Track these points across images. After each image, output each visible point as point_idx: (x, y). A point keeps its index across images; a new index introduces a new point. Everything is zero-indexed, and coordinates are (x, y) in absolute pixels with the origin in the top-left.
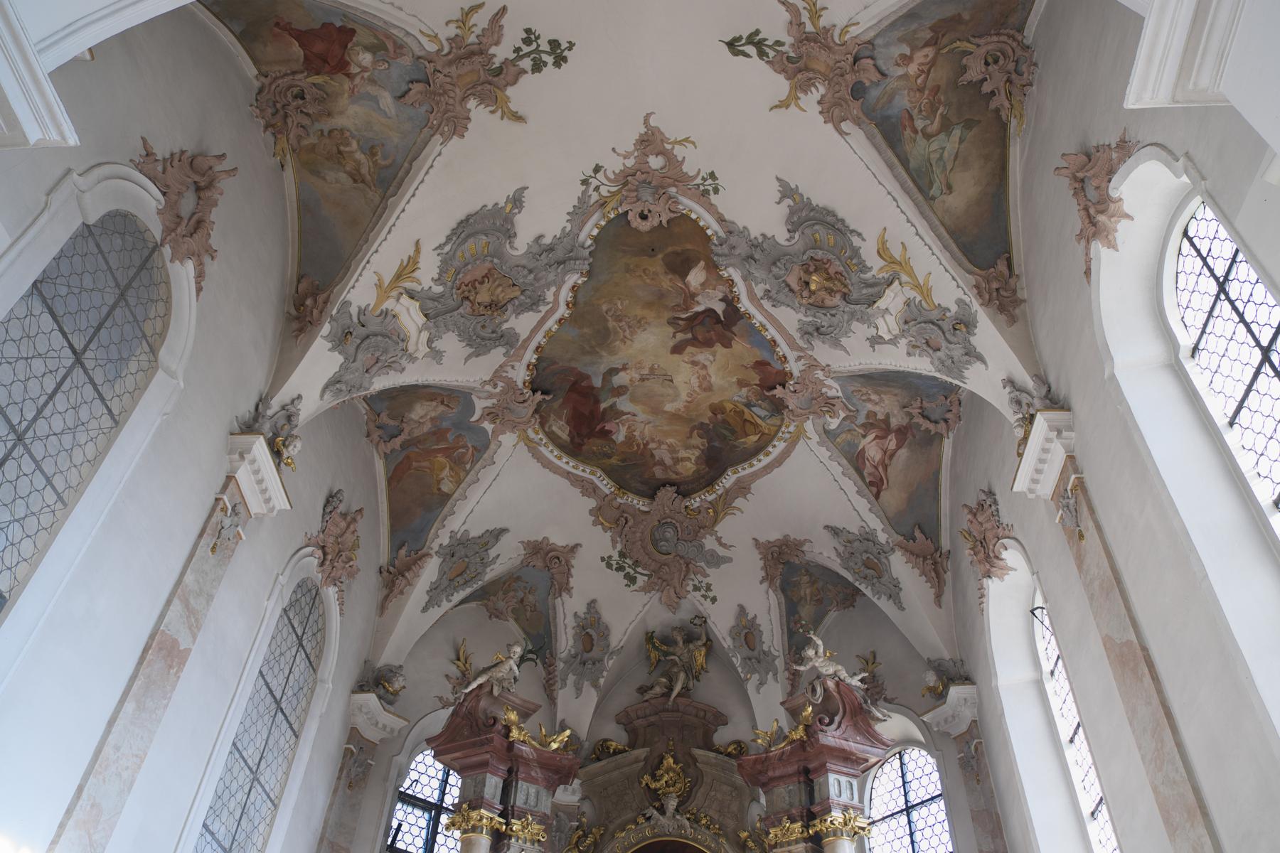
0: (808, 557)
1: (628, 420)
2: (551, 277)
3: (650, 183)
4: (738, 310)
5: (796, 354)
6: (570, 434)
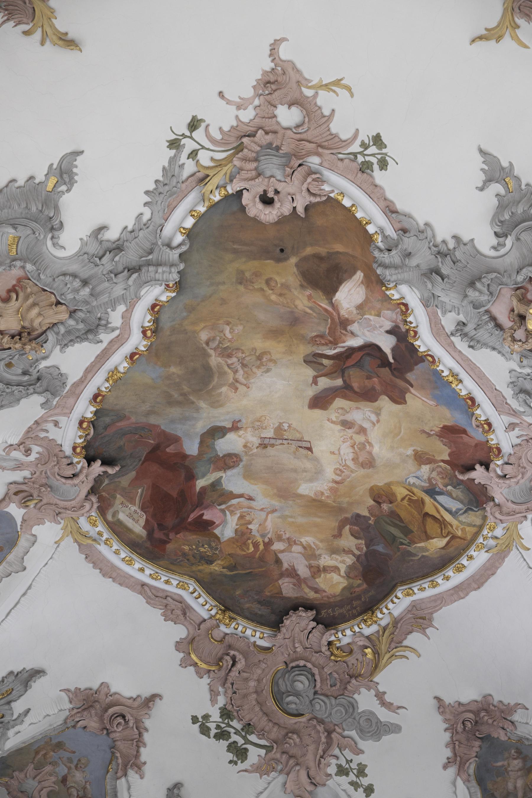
0: (522, 731)
1: (239, 506)
2: (118, 290)
3: (278, 148)
4: (414, 350)
5: (508, 419)
6: (147, 526)
